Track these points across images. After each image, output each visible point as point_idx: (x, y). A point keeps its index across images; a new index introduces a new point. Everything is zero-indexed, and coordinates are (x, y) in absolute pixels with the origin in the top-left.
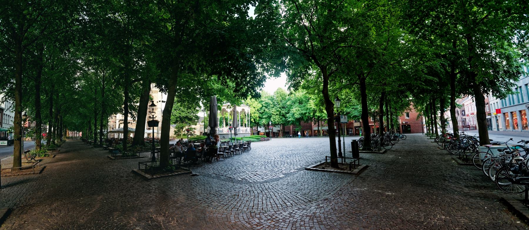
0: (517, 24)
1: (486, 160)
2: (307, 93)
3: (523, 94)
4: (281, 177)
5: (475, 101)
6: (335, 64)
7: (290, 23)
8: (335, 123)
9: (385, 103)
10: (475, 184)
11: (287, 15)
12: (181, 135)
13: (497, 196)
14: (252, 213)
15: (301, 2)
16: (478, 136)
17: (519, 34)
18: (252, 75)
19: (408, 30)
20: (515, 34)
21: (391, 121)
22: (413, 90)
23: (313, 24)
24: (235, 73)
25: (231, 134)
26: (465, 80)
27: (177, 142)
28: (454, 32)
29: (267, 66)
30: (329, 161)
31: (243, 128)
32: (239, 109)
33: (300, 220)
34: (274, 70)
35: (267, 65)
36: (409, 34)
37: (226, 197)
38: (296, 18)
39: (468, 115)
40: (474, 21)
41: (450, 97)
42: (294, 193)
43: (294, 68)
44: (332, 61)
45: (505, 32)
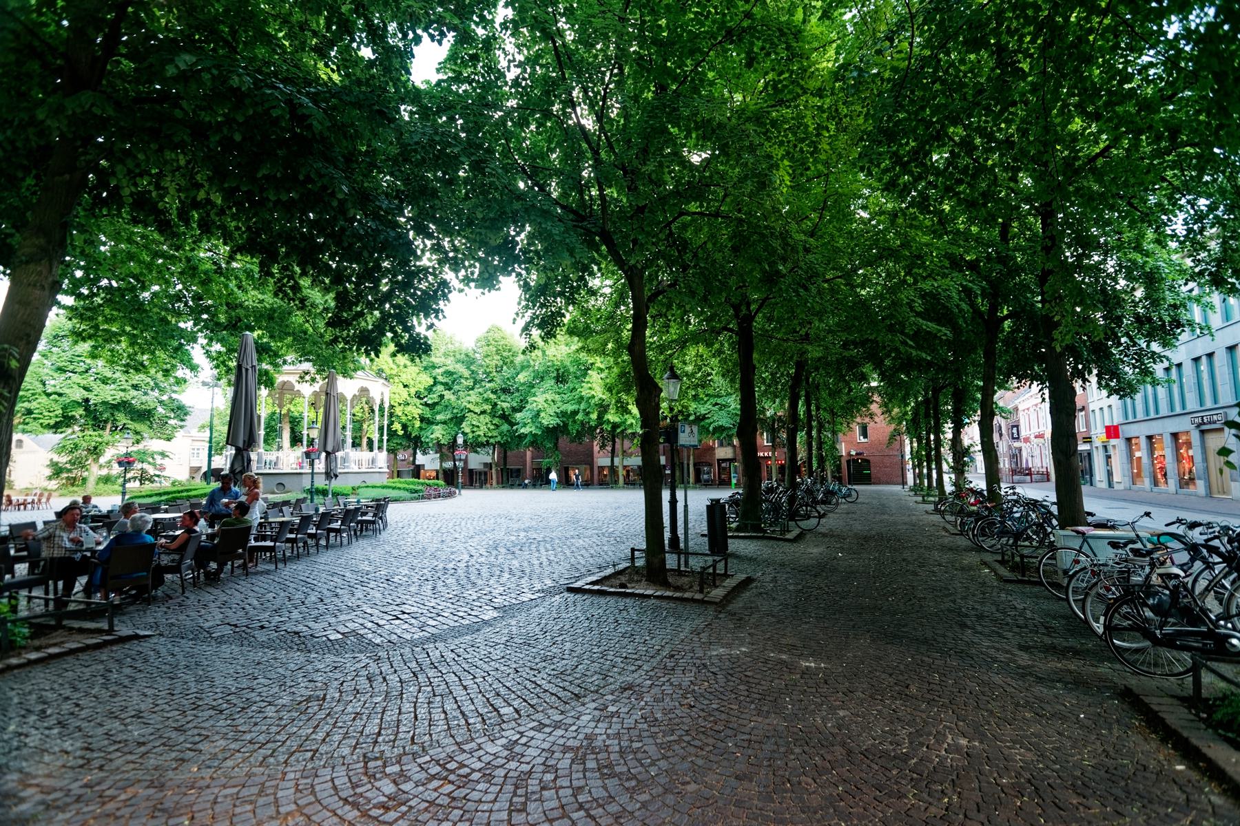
0: (1191, 177)
1: (1076, 572)
2: (583, 348)
3: (1185, 388)
4: (486, 618)
5: (1047, 400)
6: (670, 266)
7: (533, 112)
8: (661, 447)
9: (803, 393)
10: (1047, 640)
11: (524, 79)
12: (84, 480)
13: (1111, 681)
14: (371, 760)
15: (573, 41)
16: (1055, 500)
17: (1193, 208)
18: (401, 273)
19: (880, 180)
20: (1181, 208)
21: (820, 448)
22: (882, 361)
23: (607, 127)
24: (334, 260)
25: (312, 474)
26: (1026, 338)
27: (59, 515)
28: (1008, 195)
29: (456, 250)
30: (640, 563)
31: (364, 455)
32: (346, 387)
33: (542, 768)
34: (477, 264)
35: (454, 245)
36: (883, 190)
37: (270, 712)
38: (555, 96)
39: (1027, 440)
40: (1068, 163)
41: (981, 384)
42: (527, 670)
43: (545, 267)
44: (660, 256)
45: (1152, 200)
